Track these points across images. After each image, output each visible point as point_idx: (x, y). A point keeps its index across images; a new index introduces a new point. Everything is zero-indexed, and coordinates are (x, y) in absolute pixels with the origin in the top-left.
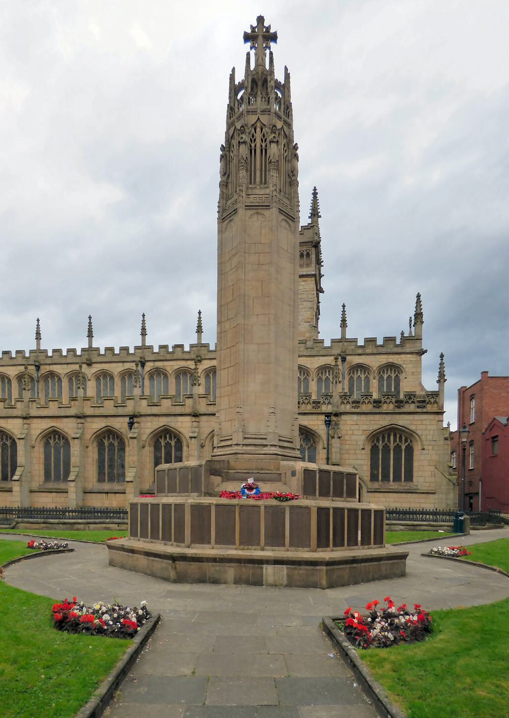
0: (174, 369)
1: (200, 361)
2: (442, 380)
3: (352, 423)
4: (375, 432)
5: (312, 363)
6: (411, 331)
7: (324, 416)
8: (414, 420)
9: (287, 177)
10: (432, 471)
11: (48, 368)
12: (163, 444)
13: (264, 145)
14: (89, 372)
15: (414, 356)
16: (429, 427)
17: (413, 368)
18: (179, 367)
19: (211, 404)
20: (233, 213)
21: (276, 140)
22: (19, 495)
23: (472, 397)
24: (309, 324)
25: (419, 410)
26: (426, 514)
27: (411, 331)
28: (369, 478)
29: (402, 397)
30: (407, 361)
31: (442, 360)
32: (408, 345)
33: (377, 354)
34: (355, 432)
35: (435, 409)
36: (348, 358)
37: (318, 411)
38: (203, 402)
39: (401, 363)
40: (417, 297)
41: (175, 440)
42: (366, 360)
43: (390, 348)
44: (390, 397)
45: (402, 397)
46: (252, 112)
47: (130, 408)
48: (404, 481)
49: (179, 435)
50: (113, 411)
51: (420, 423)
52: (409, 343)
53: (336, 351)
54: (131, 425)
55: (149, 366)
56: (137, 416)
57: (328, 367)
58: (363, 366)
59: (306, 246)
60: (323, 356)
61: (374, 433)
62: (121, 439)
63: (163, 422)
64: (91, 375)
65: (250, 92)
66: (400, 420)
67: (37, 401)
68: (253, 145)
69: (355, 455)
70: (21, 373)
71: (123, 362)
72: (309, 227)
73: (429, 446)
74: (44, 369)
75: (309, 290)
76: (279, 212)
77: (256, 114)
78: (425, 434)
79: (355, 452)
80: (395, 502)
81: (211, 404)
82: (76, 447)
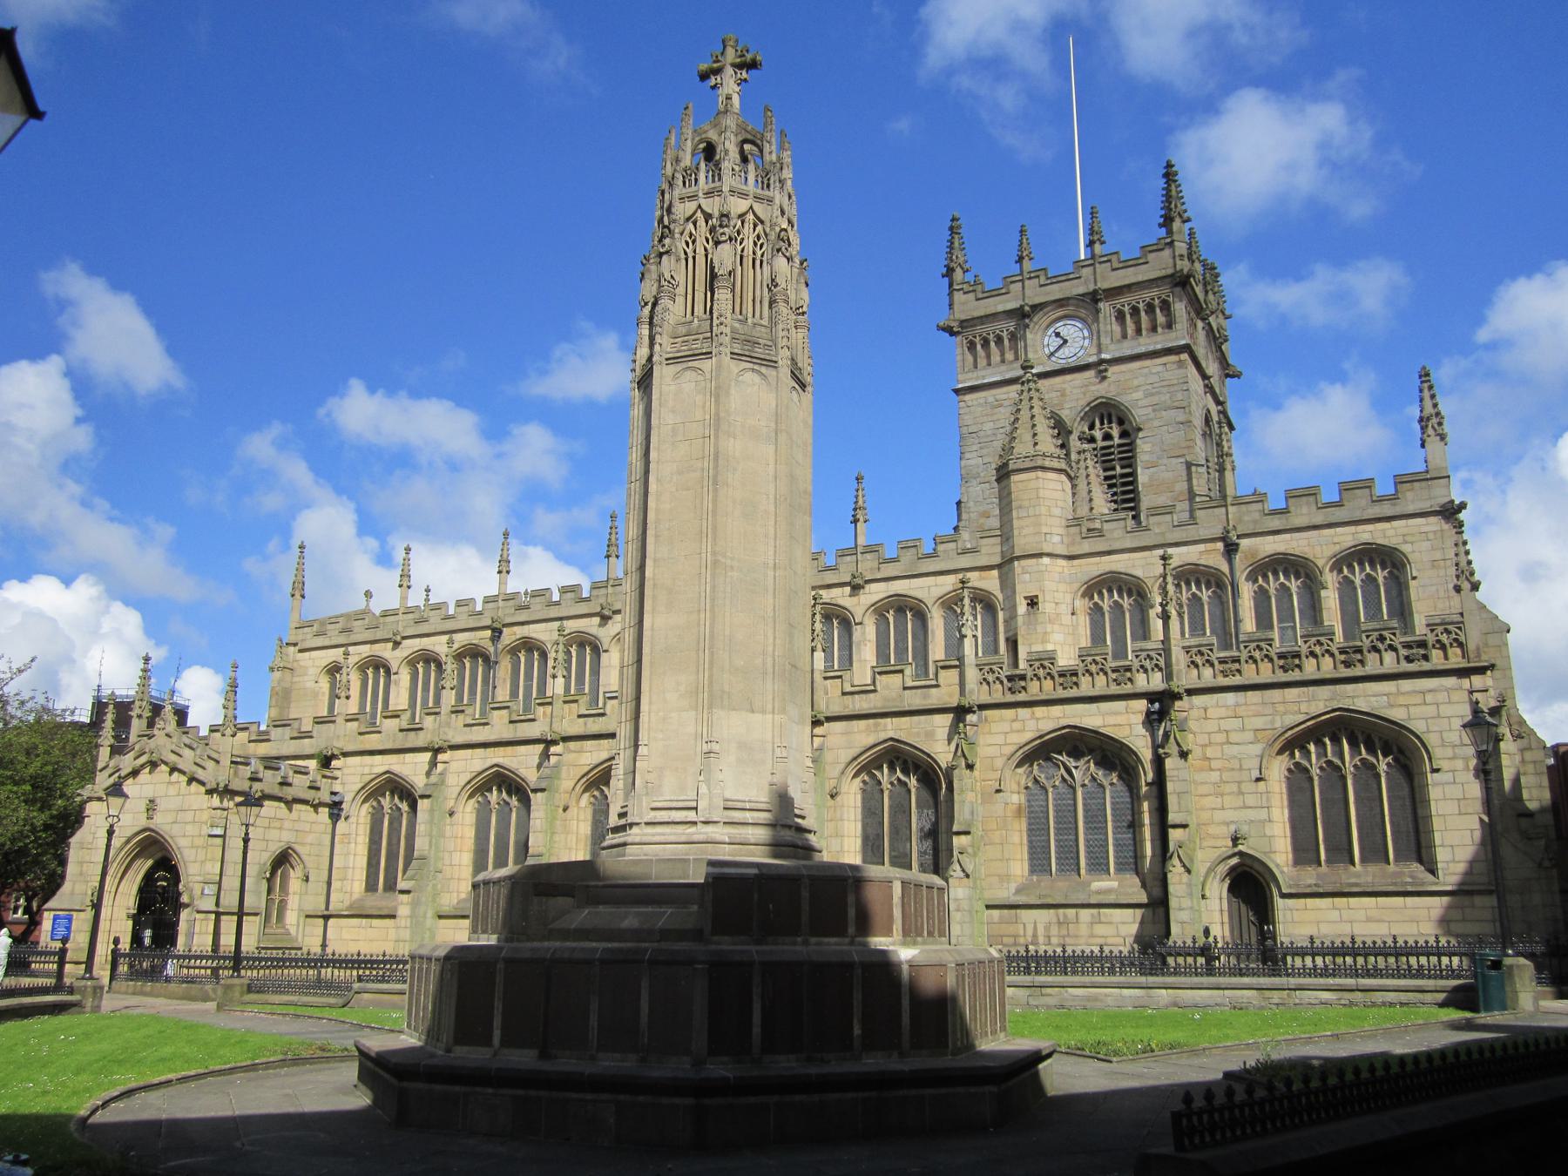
3: (1222, 712)
4: (1290, 733)
5: (1148, 564)
8: (1399, 693)
10: (1472, 830)
11: (520, 632)
13: (759, 253)
15: (1433, 519)
16: (1446, 710)
17: (1433, 549)
22: (408, 925)
24: (1182, 460)
25: (1406, 667)
26: (1408, 955)
28: (1290, 856)
30: (1412, 535)
32: (1409, 495)
34: (1234, 737)
35: (1456, 659)
36: (1244, 543)
37: (1127, 688)
38: (834, 687)
42: (1294, 544)
43: (1358, 505)
44: (1322, 639)
51: (1418, 699)
58: (1289, 560)
59: (1158, 287)
61: (1287, 735)
63: (380, 764)
64: (610, 639)
66: (1358, 696)
67: (466, 712)
68: (690, 252)
69: (1241, 797)
70: (463, 646)
72: (1160, 247)
73: (1456, 761)
74: (510, 636)
75: (1175, 382)
78: (1436, 729)
79: (1239, 787)
80: (1369, 920)
82: (538, 810)
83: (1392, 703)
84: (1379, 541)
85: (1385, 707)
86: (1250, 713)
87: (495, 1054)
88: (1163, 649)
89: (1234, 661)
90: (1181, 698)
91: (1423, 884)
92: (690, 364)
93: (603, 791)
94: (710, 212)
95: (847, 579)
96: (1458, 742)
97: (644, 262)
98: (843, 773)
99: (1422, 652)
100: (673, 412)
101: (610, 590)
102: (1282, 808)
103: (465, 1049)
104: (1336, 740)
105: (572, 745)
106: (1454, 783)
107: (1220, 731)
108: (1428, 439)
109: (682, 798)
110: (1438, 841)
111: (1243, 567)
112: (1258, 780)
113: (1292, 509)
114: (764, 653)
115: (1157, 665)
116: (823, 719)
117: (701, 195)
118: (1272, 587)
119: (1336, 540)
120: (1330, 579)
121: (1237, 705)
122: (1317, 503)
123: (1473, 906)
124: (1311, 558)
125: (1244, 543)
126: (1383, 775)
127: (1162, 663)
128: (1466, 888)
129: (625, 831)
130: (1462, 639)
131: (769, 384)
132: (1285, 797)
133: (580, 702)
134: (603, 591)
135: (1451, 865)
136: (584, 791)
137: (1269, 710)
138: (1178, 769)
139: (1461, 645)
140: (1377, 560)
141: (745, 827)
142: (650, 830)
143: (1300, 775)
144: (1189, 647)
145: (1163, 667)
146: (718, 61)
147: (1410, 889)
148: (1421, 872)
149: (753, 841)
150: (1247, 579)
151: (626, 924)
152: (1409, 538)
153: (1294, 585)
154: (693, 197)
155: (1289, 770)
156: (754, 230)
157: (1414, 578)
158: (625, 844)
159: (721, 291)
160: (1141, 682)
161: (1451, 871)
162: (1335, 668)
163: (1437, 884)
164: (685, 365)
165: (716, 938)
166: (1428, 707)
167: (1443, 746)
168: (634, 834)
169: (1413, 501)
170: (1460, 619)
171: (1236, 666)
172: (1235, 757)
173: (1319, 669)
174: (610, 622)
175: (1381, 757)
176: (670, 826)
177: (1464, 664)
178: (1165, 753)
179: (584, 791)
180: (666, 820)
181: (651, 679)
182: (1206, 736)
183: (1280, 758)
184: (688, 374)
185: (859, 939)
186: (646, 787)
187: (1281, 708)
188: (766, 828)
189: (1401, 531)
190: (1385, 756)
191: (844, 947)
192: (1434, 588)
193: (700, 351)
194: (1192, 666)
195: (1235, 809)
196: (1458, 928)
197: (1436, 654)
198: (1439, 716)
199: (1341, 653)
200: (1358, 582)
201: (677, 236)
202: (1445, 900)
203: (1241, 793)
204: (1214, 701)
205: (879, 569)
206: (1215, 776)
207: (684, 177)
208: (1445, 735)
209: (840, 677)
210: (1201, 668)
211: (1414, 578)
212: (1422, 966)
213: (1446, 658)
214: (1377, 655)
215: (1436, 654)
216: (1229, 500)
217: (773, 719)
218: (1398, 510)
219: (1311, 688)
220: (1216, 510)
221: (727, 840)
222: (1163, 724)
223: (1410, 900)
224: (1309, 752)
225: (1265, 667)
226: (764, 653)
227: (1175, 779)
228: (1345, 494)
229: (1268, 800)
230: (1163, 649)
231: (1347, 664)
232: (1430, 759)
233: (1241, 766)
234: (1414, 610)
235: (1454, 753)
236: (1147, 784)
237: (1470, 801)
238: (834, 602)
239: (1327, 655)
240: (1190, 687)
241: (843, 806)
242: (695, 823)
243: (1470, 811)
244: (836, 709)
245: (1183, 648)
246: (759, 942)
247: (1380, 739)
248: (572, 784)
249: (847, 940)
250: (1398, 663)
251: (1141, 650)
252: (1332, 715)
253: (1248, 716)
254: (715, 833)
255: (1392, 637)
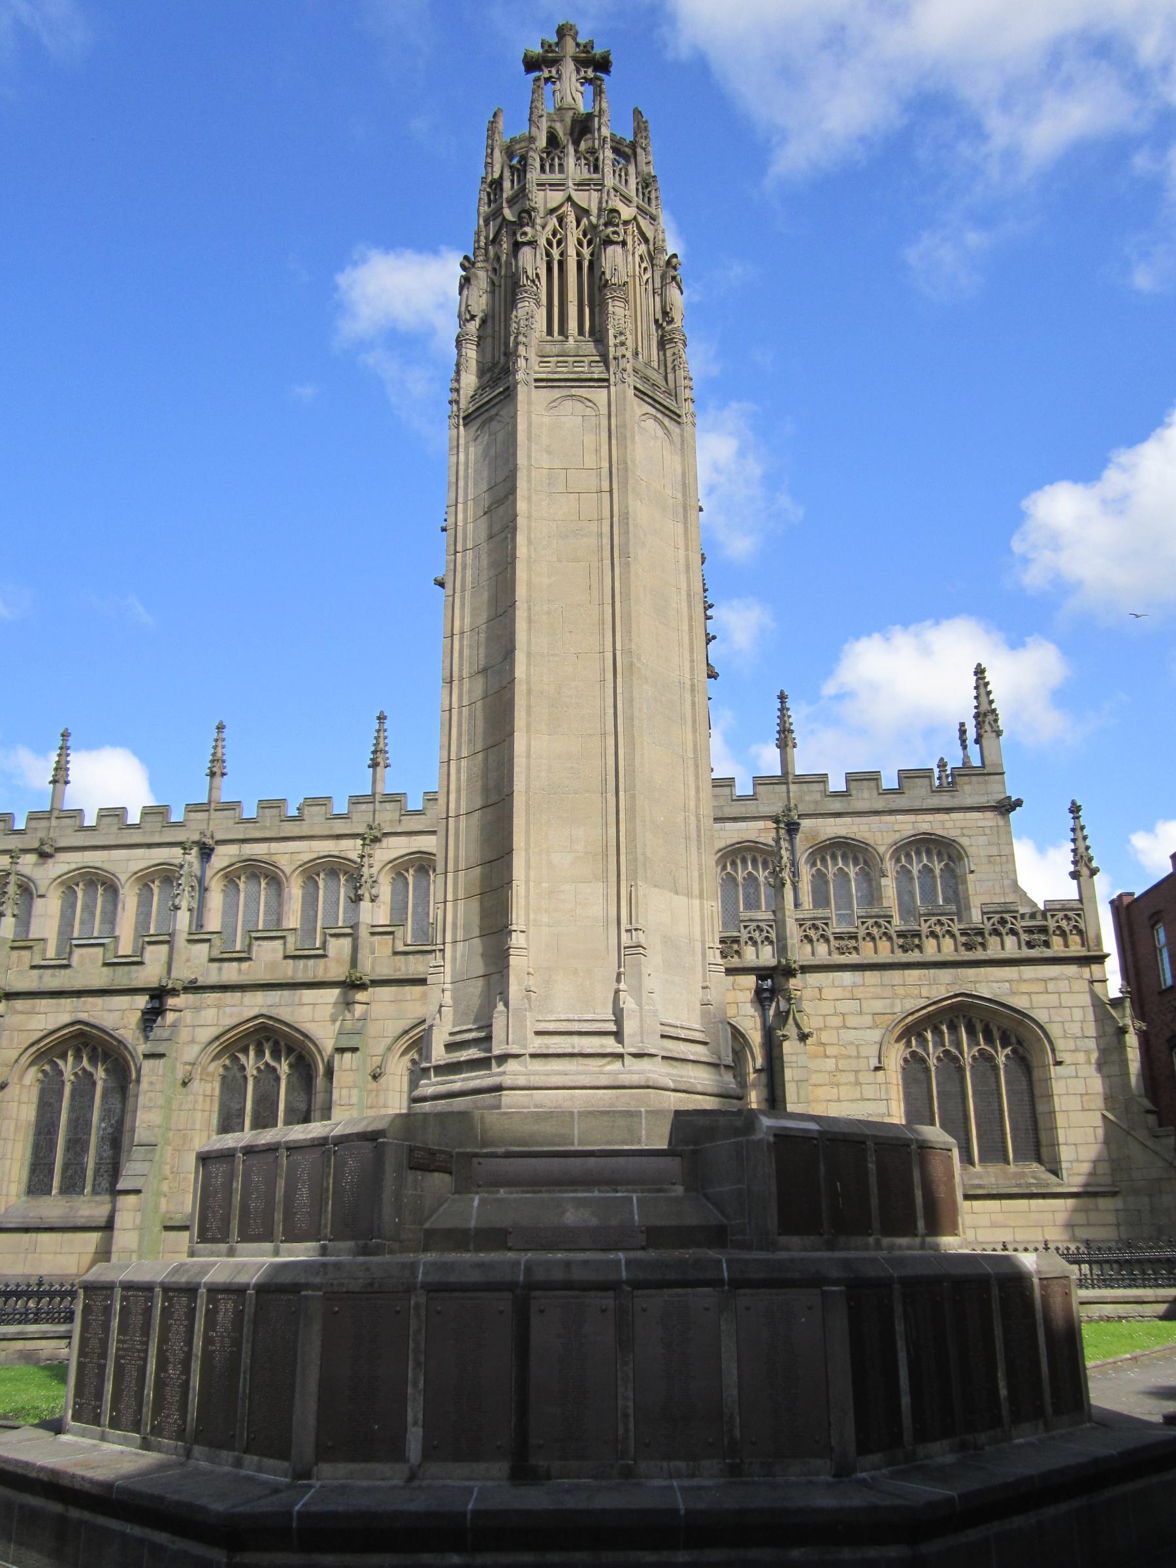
0: (300, 863)
1: (376, 840)
2: (1085, 872)
3: (838, 992)
4: (910, 1018)
6: (966, 757)
7: (753, 978)
9: (653, 327)
12: (251, 1071)
14: (46, 874)
15: (989, 815)
16: (1067, 1000)
18: (315, 856)
19: (406, 953)
20: (497, 400)
21: (621, 239)
23: (1155, 918)
27: (966, 757)
29: (976, 916)
31: (1076, 818)
32: (967, 788)
33: (883, 812)
34: (851, 1021)
35: (1076, 948)
36: (805, 823)
38: (383, 946)
39: (952, 833)
40: (976, 673)
41: (292, 1058)
42: (855, 829)
43: (919, 794)
45: (976, 916)
46: (551, 185)
47: (151, 973)
48: (1015, 1160)
49: (304, 1047)
50: (100, 978)
51: (1040, 987)
52: (970, 783)
53: (773, 803)
54: (152, 1016)
55: (223, 856)
56: (174, 989)
57: (748, 849)
58: (848, 844)
60: (735, 819)
61: (907, 1021)
62: (116, 1059)
63: (254, 1004)
64: (47, 882)
65: (546, 148)
66: (980, 982)
68: (555, 253)
69: (858, 1088)
71: (149, 846)
76: (635, 395)
77: (563, 190)
78: (1058, 1019)
79: (857, 1078)
80: (994, 1225)
81: (406, 953)
83: (1015, 990)
84: (939, 832)
85: (1006, 995)
86: (869, 995)
87: (412, 1477)
88: (774, 920)
89: (850, 938)
90: (794, 976)
91: (1048, 1185)
92: (574, 391)
93: (57, 1065)
94: (585, 206)
95: (361, 829)
96: (1079, 1035)
97: (467, 264)
98: (389, 1049)
99: (1043, 938)
100: (549, 453)
101: (54, 822)
102: (899, 1101)
103: (343, 1468)
104: (953, 1028)
105: (19, 1004)
106: (1077, 1077)
107: (835, 1014)
108: (985, 735)
109: (589, 1017)
110: (1061, 1140)
111: (803, 848)
112: (877, 1069)
113: (854, 792)
114: (685, 808)
115: (767, 938)
116: (368, 982)
117: (571, 184)
118: (831, 871)
119: (897, 827)
120: (889, 866)
121: (854, 986)
122: (878, 789)
123: (1097, 1210)
124: (872, 843)
125: (805, 823)
126: (968, 1068)
127: (773, 936)
128: (1090, 1189)
129: (489, 1067)
130: (1082, 926)
131: (672, 442)
132: (901, 1088)
133: (36, 949)
134: (44, 823)
135: (1074, 1164)
136: (32, 1064)
137: (887, 992)
138: (797, 1054)
139: (1080, 932)
140: (935, 852)
141: (684, 1065)
142: (538, 1066)
143: (916, 1066)
144: (803, 919)
145: (775, 940)
146: (553, 51)
147: (1035, 1191)
148: (1042, 1172)
149: (700, 1088)
150: (806, 862)
151: (571, 1217)
152: (966, 832)
153: (852, 871)
154: (555, 186)
155: (905, 1060)
156: (578, 226)
157: (972, 872)
158: (499, 1088)
159: (617, 303)
160: (750, 956)
161: (1075, 1171)
162: (956, 950)
163: (1061, 1185)
164: (565, 392)
165: (783, 1240)
166: (1075, 996)
167: (1065, 1037)
168: (512, 1072)
169: (970, 795)
170: (1080, 906)
171: (853, 943)
172: (852, 1043)
173: (939, 951)
174: (50, 861)
175: (999, 1049)
176: (575, 1060)
177: (1084, 952)
178: (784, 1036)
179: (32, 1064)
180: (569, 1051)
181: (528, 832)
182: (821, 1018)
183: (897, 1045)
184: (569, 404)
185: (929, 1239)
186: (529, 999)
187: (901, 991)
188: (711, 1069)
189: (958, 824)
190: (1004, 1047)
191: (916, 1252)
192: (990, 884)
193: (589, 376)
194: (805, 941)
195: (852, 1101)
196: (1083, 1233)
197: (1057, 941)
198: (1061, 1006)
199: (962, 934)
200: (915, 872)
201: (539, 228)
202: (1070, 1202)
203: (858, 1083)
204: (830, 980)
205: (400, 821)
206: (830, 1064)
207: (542, 159)
208: (1067, 1026)
209: (392, 933)
210: (815, 943)
211: (972, 872)
212: (1085, 1275)
213: (1066, 945)
214: (998, 939)
215: (1057, 941)
216: (791, 777)
217: (702, 908)
218: (955, 803)
219: (932, 971)
220: (776, 786)
221: (672, 1085)
222: (774, 1004)
223: (1034, 1202)
224: (925, 1040)
225: (884, 945)
226: (685, 808)
227: (794, 1065)
228: (906, 782)
229: (887, 1091)
230: (774, 920)
231: (969, 947)
232: (1053, 1050)
233: (858, 1052)
234: (972, 905)
235: (1076, 1046)
236: (756, 1071)
237: (1092, 1097)
238: (343, 854)
239: (947, 937)
240: (805, 963)
241: (387, 1089)
242: (620, 1056)
243: (1093, 1106)
244: (384, 972)
245: (797, 920)
246: (831, 1246)
247: (999, 1028)
248: (14, 1054)
249: (918, 1240)
250: (1020, 948)
251: (751, 920)
252: (954, 1000)
253: (865, 999)
254: (654, 1072)
255: (950, 923)
